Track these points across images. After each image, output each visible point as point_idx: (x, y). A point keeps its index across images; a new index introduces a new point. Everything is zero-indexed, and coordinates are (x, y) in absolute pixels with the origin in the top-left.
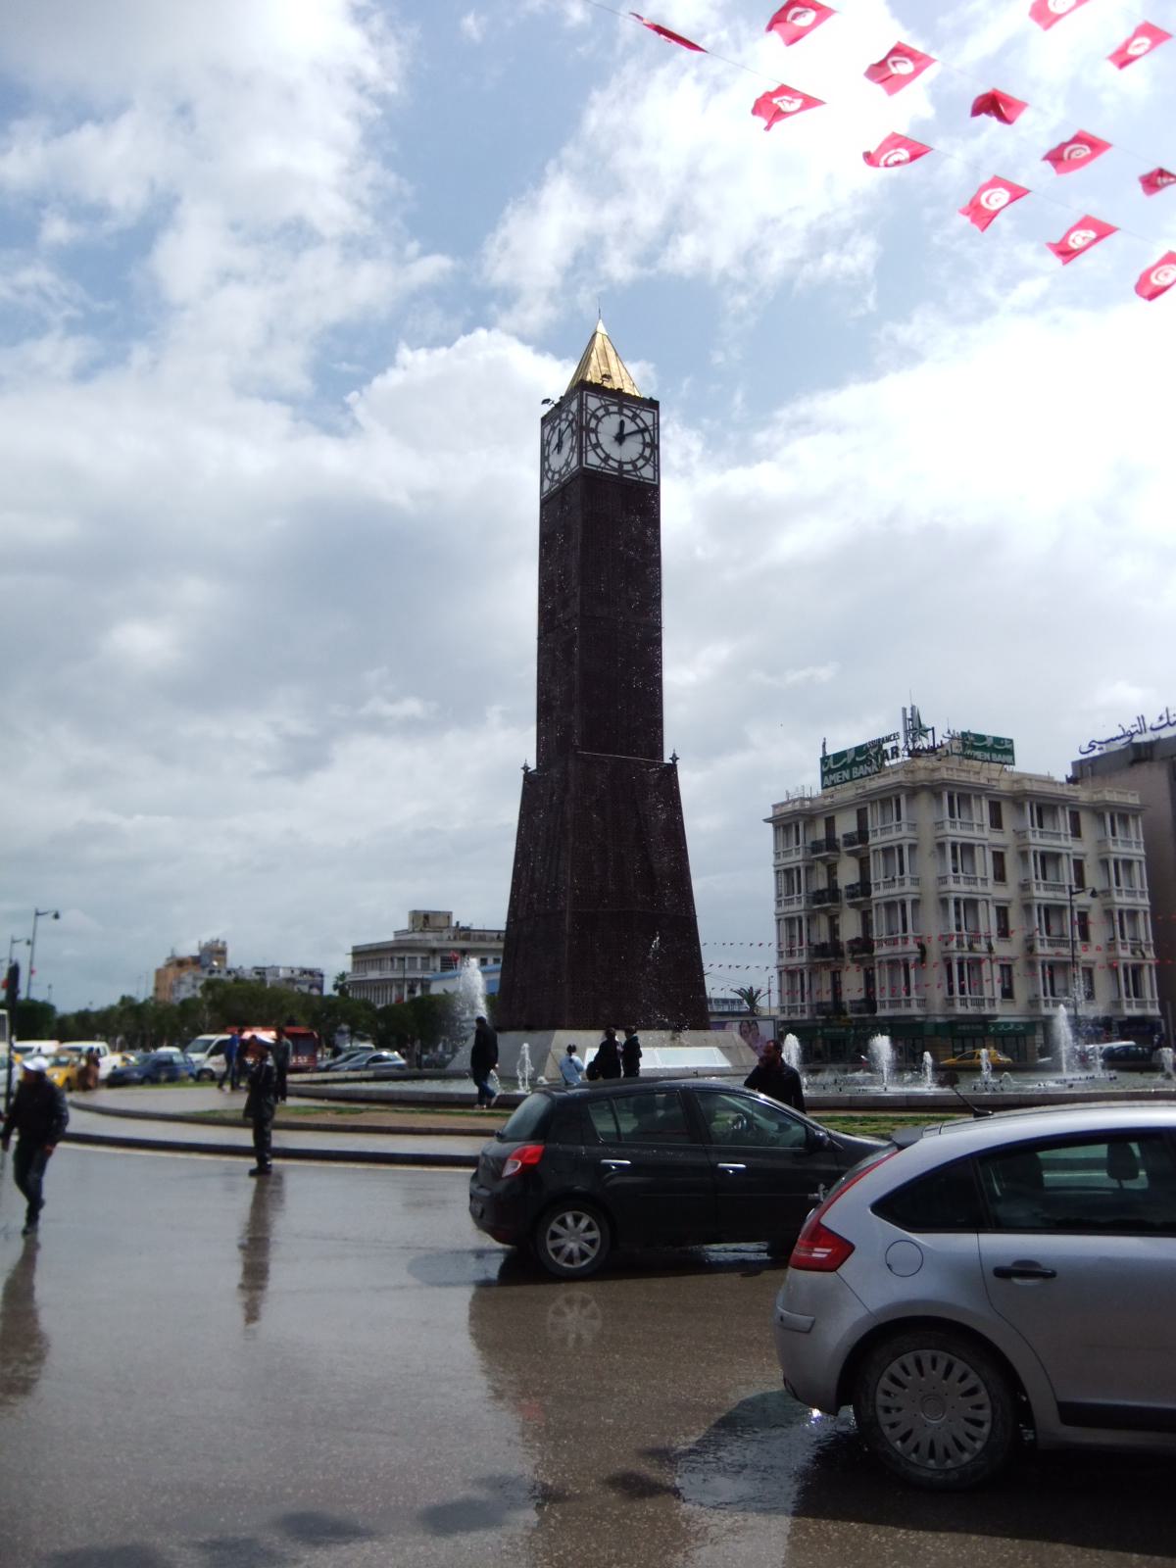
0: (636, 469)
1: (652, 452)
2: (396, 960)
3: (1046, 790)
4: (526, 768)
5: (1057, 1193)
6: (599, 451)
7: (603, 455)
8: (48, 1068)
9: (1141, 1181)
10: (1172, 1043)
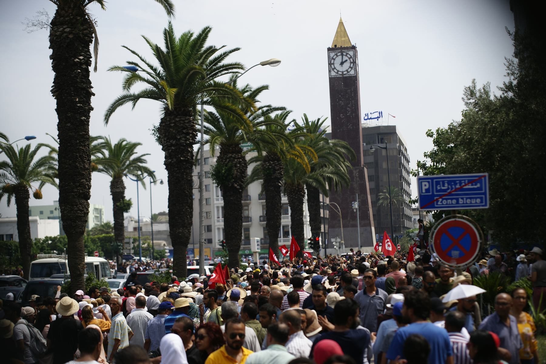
0: (348, 72)
5: (39, 163)
7: (336, 71)
9: (388, 240)
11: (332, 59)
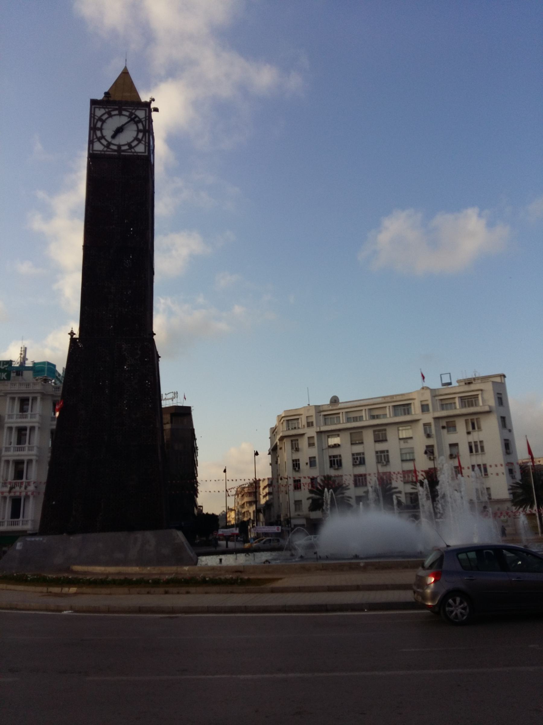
1: (95, 125)
2: (344, 413)
3: (431, 406)
4: (72, 334)
8: (11, 486)
10: (167, 418)
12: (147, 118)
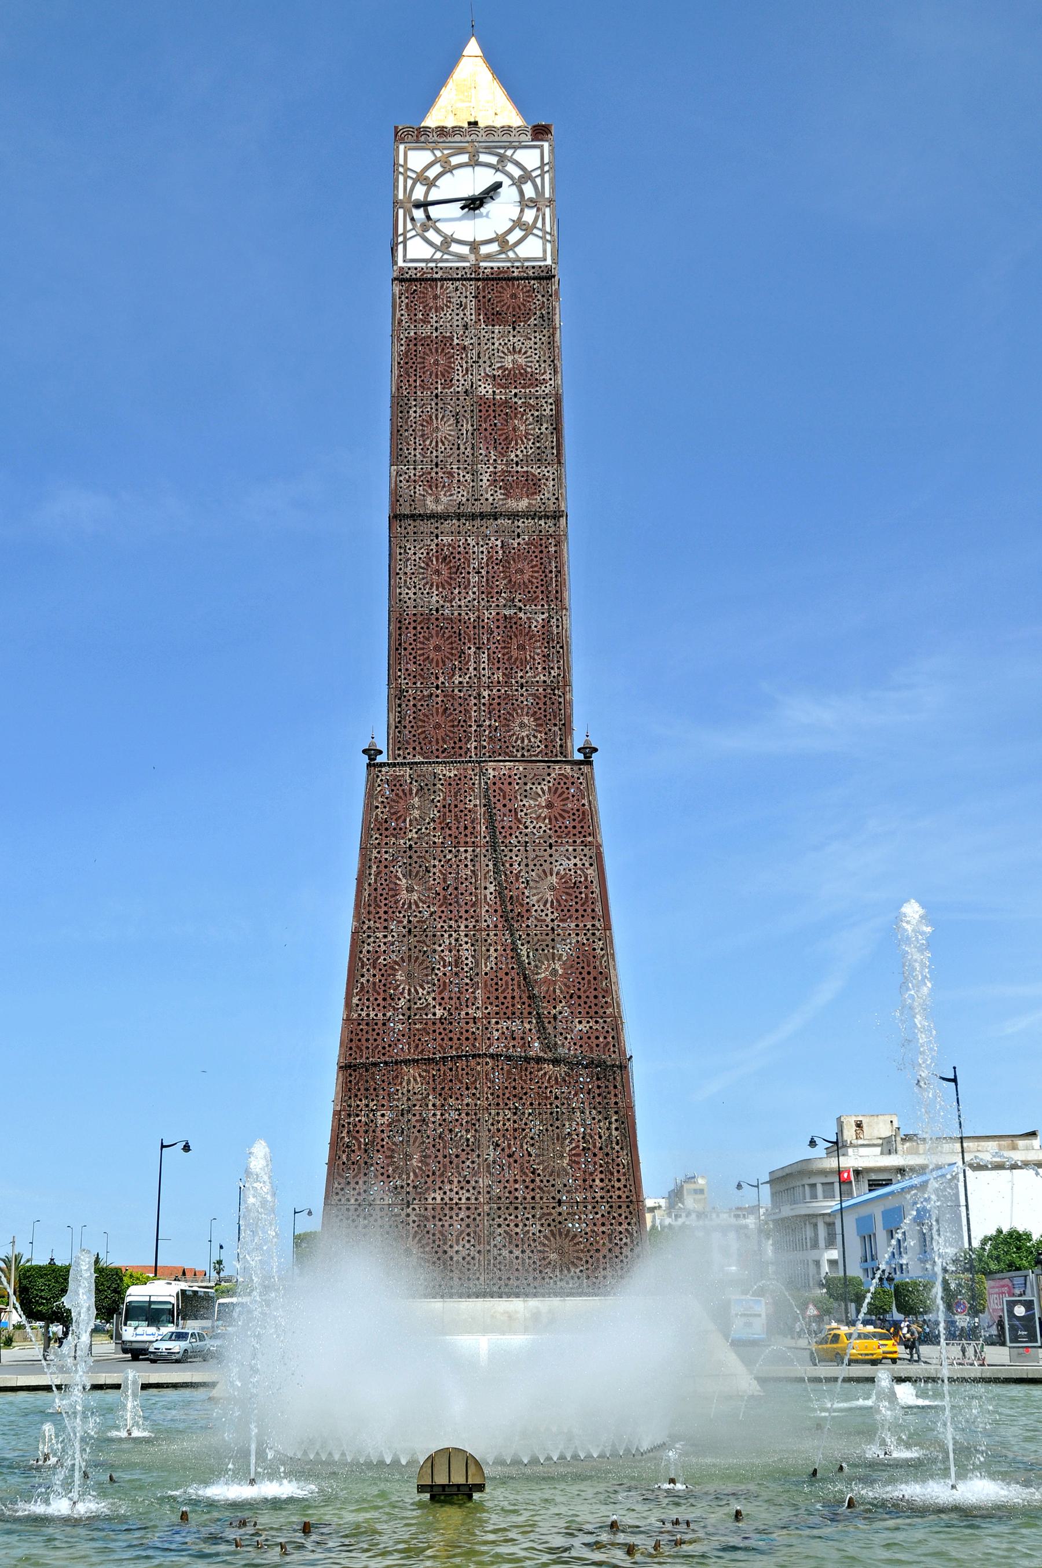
6: (431, 235)
7: (437, 240)
11: (534, 226)
12: (401, 239)
